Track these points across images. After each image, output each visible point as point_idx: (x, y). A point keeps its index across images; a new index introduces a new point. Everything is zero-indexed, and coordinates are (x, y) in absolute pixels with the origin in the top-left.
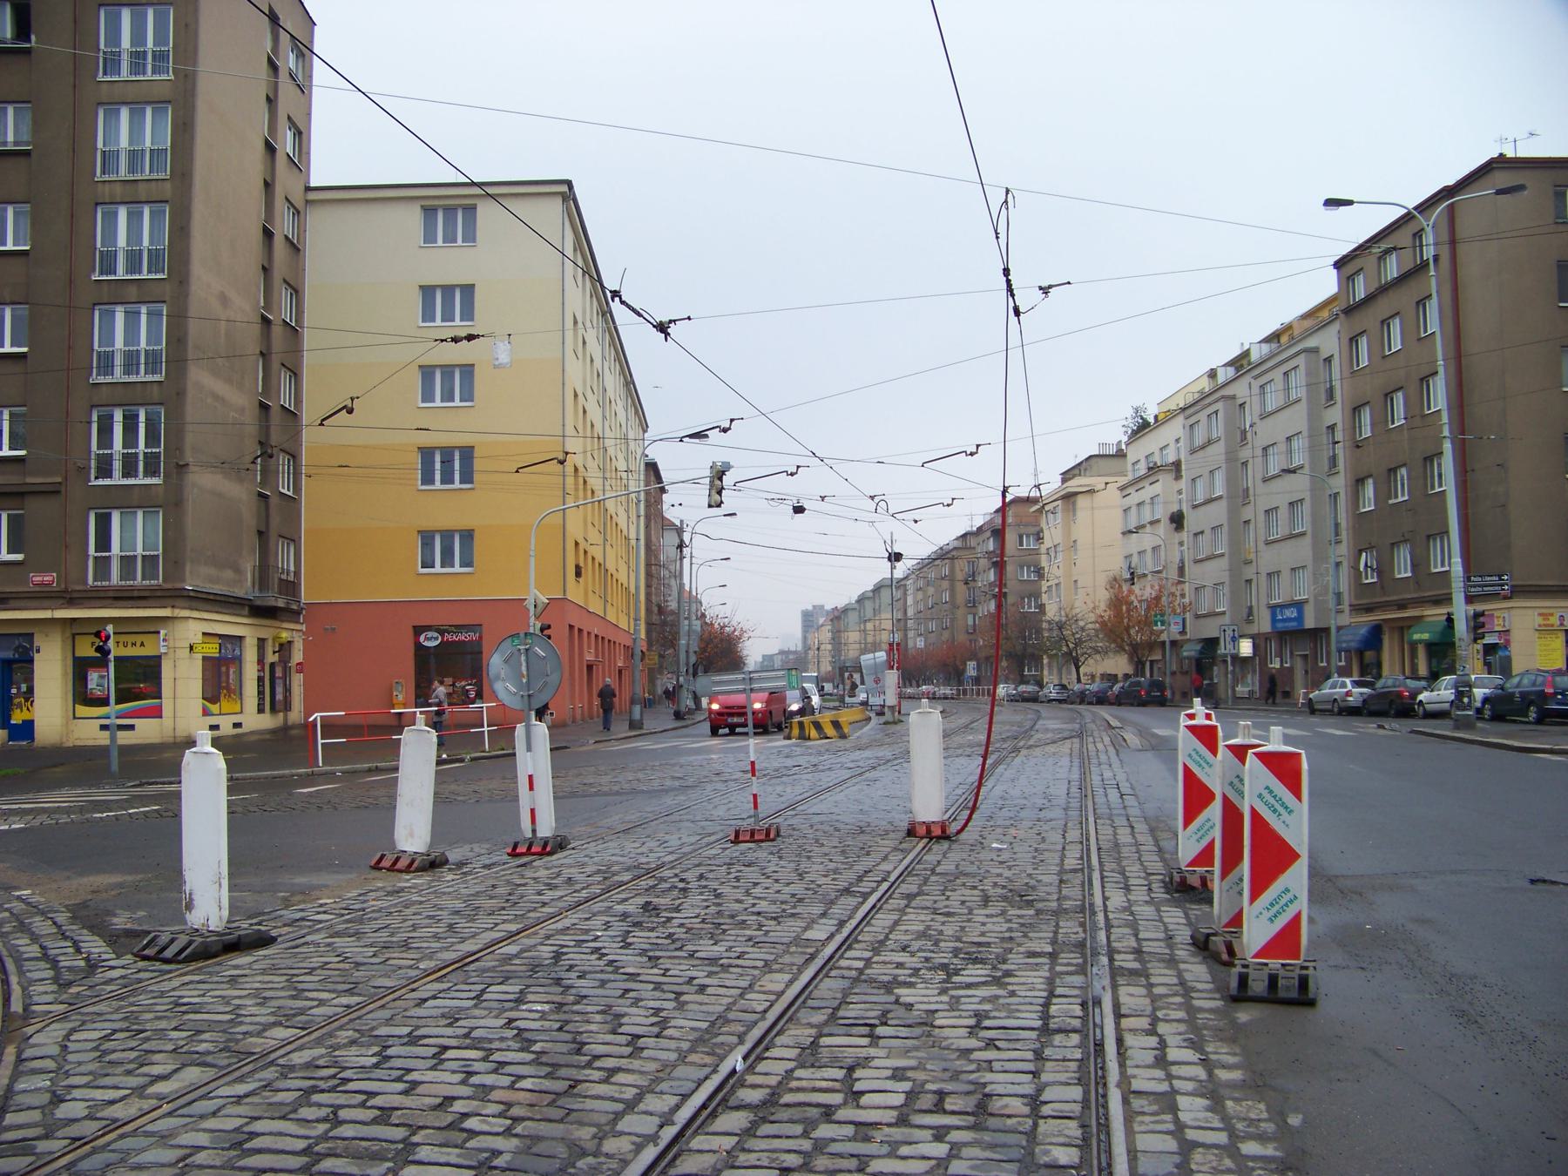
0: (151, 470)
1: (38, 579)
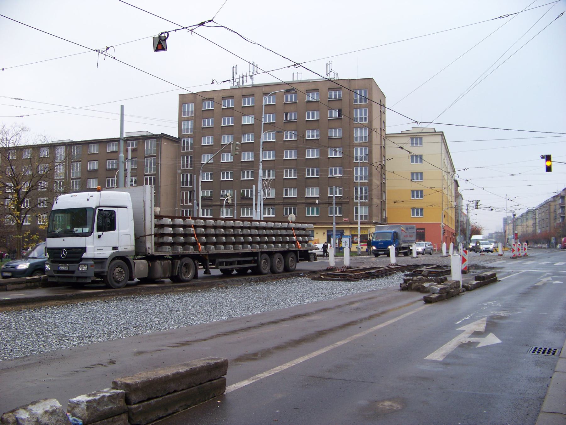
0: (366, 199)
1: (345, 220)
